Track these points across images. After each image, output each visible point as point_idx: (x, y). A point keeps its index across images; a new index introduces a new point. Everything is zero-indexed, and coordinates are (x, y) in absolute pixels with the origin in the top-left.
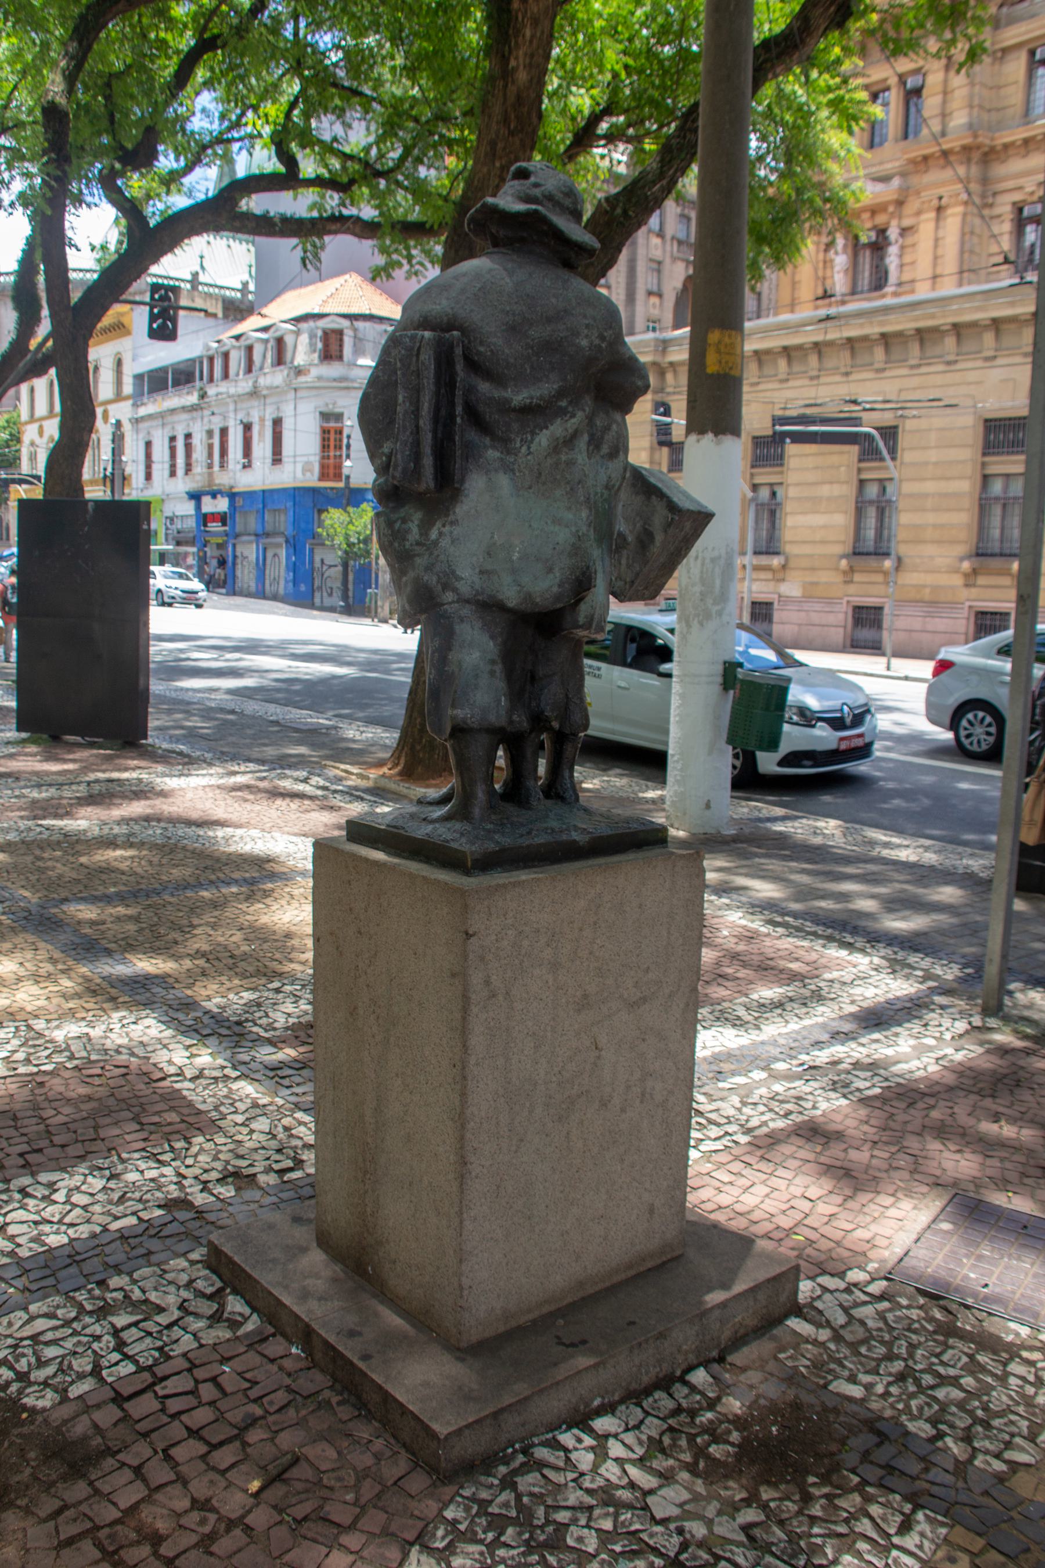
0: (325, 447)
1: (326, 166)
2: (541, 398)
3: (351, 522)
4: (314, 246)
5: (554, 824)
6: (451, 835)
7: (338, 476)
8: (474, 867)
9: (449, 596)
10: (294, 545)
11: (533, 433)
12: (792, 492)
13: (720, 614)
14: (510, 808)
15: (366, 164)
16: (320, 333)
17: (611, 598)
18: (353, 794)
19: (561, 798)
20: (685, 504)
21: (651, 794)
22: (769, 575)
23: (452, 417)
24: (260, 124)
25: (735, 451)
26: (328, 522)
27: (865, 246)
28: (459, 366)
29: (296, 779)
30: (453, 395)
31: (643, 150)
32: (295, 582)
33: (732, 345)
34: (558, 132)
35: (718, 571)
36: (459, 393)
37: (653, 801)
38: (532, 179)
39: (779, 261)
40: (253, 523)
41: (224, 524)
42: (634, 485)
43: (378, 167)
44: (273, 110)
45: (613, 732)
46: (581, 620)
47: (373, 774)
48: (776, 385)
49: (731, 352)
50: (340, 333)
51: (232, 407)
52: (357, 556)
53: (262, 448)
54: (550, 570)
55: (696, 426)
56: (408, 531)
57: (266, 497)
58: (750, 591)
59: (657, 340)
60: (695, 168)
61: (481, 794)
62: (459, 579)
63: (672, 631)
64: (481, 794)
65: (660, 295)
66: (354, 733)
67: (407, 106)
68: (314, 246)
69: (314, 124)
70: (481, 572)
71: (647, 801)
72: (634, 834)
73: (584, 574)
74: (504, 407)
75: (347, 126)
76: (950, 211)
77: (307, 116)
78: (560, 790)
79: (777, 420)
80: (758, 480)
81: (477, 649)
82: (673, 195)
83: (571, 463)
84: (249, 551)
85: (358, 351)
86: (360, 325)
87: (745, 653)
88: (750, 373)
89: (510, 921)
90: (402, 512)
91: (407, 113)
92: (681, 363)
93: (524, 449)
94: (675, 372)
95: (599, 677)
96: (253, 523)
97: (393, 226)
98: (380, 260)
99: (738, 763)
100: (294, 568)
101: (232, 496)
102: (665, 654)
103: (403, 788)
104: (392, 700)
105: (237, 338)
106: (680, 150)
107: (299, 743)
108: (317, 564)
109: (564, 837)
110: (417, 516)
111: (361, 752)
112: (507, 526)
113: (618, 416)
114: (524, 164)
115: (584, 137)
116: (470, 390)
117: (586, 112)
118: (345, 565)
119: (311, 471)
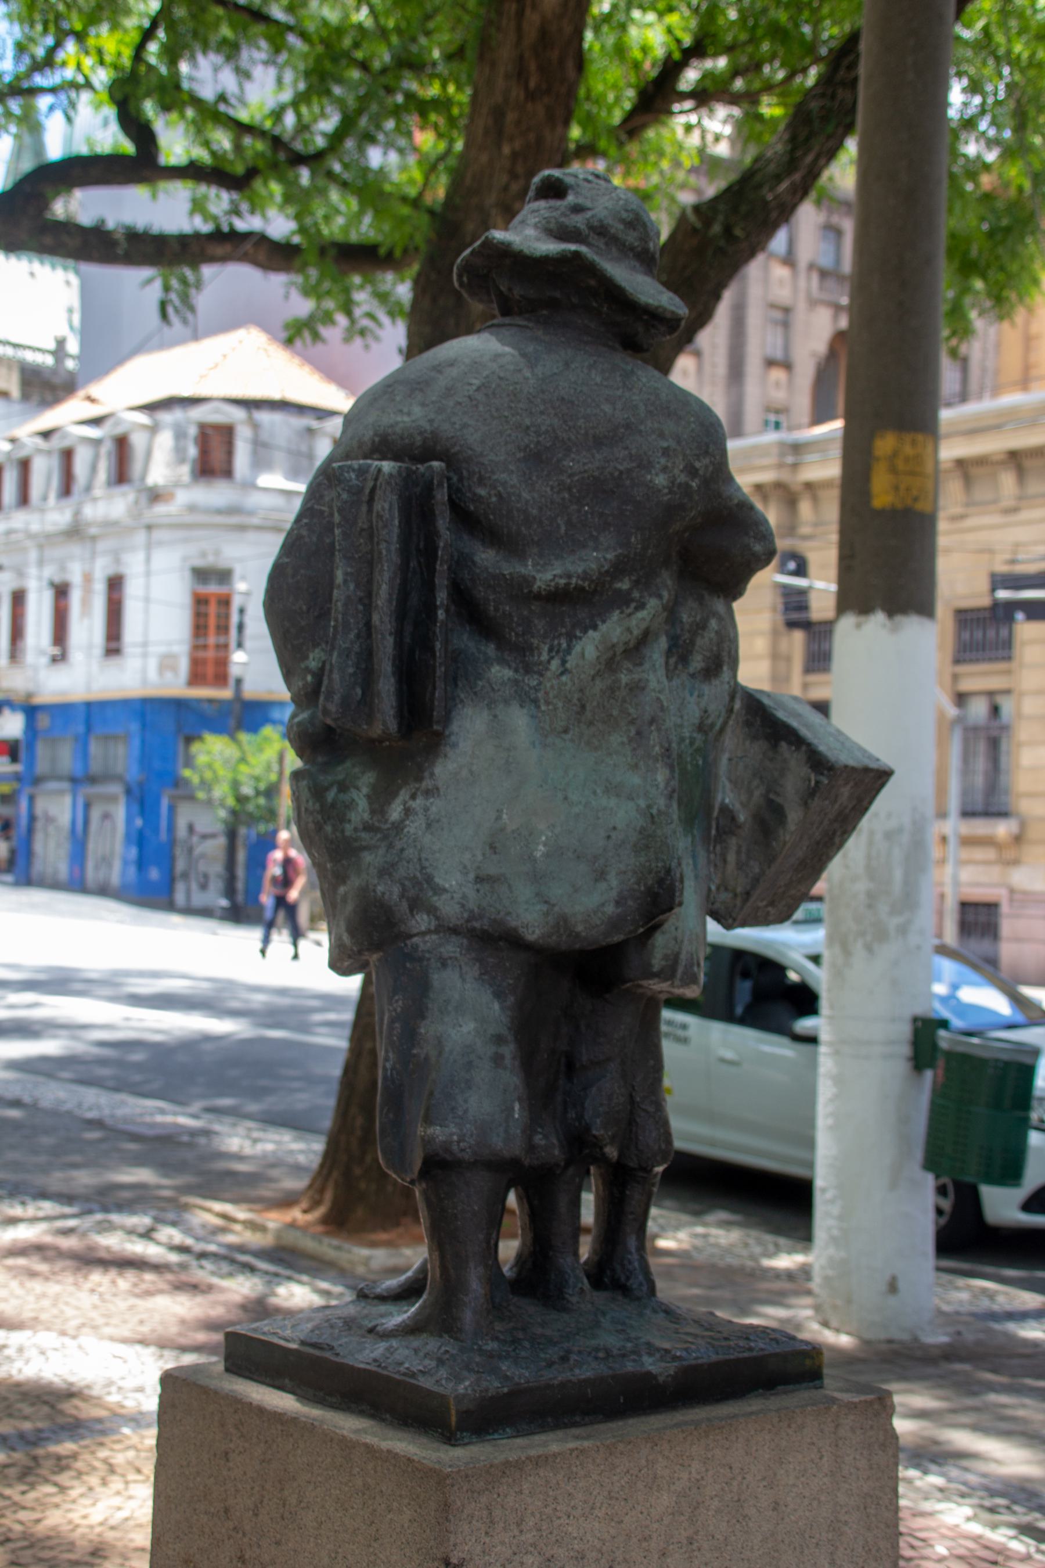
0: (199, 627)
1: (206, 144)
2: (585, 576)
3: (243, 760)
4: (184, 281)
5: (611, 1340)
6: (417, 1361)
7: (221, 678)
8: (461, 1428)
9: (422, 921)
10: (141, 799)
11: (571, 637)
12: (1030, 706)
13: (903, 930)
14: (529, 1309)
15: (276, 142)
16: (193, 431)
17: (709, 919)
18: (235, 1260)
19: (622, 1288)
20: (843, 758)
21: (785, 1261)
22: (990, 854)
23: (429, 608)
24: (89, 63)
25: (926, 640)
26: (202, 759)
28: (443, 523)
29: (131, 1232)
30: (432, 571)
31: (759, 118)
32: (141, 864)
33: (918, 459)
34: (610, 89)
35: (897, 854)
36: (441, 568)
37: (789, 1275)
38: (571, 198)
39: (1000, 303)
40: (66, 758)
41: (14, 758)
42: (748, 724)
43: (298, 146)
44: (113, 42)
45: (713, 1143)
46: (657, 962)
47: (274, 1220)
49: (917, 472)
50: (227, 432)
51: (33, 555)
52: (252, 819)
53: (87, 628)
54: (601, 875)
55: (854, 598)
56: (351, 805)
57: (92, 716)
58: (956, 883)
59: (782, 444)
60: (851, 146)
61: (475, 1283)
62: (439, 890)
63: (816, 959)
64: (475, 1283)
65: (787, 365)
66: (242, 1142)
67: (347, 42)
68: (184, 281)
69: (184, 67)
70: (479, 879)
71: (777, 1274)
72: (758, 1362)
73: (661, 882)
74: (521, 592)
75: (243, 74)
77: (172, 54)
78: (619, 1268)
79: (998, 581)
80: (966, 685)
81: (469, 1016)
82: (813, 195)
83: (637, 688)
84: (58, 808)
85: (261, 461)
86: (264, 417)
87: (949, 999)
88: (951, 498)
89: (529, 1537)
90: (339, 773)
91: (347, 55)
92: (826, 484)
93: (555, 664)
94: (815, 500)
95: (685, 1041)
96: (66, 758)
97: (323, 251)
98: (303, 307)
99: (946, 1204)
100: (139, 839)
101: (31, 711)
102: (804, 1000)
103: (328, 1247)
104: (311, 1081)
105: (46, 435)
106: (825, 119)
107: (138, 1160)
108: (181, 831)
109: (630, 1367)
110: (367, 780)
111: (253, 1179)
112: (525, 801)
113: (719, 605)
114: (556, 173)
115: (656, 96)
116: (461, 562)
117: (659, 53)
118: (232, 835)
119: (174, 669)
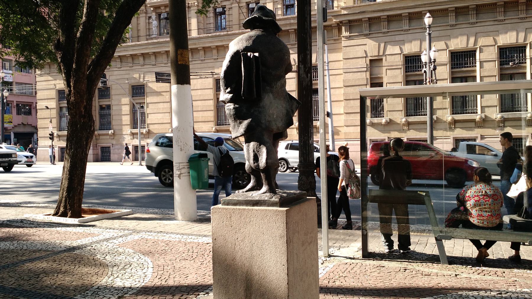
27: (163, 19)
48: (140, 67)
76: (192, 8)
